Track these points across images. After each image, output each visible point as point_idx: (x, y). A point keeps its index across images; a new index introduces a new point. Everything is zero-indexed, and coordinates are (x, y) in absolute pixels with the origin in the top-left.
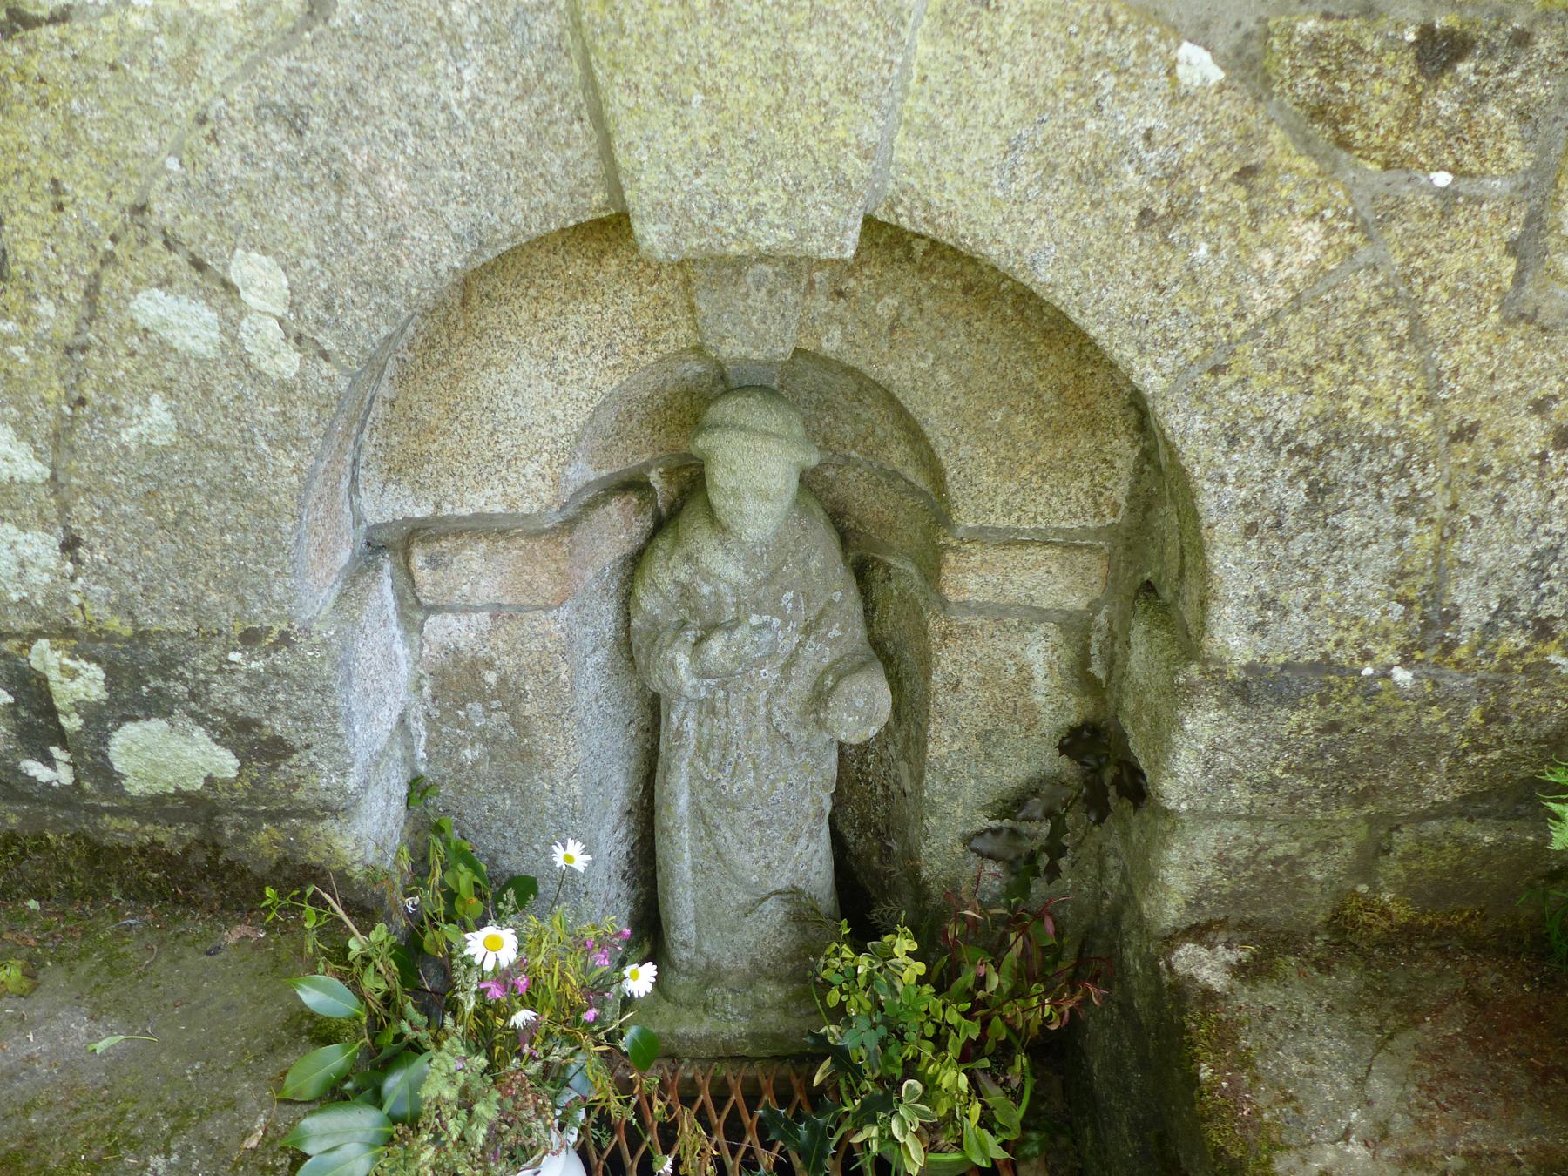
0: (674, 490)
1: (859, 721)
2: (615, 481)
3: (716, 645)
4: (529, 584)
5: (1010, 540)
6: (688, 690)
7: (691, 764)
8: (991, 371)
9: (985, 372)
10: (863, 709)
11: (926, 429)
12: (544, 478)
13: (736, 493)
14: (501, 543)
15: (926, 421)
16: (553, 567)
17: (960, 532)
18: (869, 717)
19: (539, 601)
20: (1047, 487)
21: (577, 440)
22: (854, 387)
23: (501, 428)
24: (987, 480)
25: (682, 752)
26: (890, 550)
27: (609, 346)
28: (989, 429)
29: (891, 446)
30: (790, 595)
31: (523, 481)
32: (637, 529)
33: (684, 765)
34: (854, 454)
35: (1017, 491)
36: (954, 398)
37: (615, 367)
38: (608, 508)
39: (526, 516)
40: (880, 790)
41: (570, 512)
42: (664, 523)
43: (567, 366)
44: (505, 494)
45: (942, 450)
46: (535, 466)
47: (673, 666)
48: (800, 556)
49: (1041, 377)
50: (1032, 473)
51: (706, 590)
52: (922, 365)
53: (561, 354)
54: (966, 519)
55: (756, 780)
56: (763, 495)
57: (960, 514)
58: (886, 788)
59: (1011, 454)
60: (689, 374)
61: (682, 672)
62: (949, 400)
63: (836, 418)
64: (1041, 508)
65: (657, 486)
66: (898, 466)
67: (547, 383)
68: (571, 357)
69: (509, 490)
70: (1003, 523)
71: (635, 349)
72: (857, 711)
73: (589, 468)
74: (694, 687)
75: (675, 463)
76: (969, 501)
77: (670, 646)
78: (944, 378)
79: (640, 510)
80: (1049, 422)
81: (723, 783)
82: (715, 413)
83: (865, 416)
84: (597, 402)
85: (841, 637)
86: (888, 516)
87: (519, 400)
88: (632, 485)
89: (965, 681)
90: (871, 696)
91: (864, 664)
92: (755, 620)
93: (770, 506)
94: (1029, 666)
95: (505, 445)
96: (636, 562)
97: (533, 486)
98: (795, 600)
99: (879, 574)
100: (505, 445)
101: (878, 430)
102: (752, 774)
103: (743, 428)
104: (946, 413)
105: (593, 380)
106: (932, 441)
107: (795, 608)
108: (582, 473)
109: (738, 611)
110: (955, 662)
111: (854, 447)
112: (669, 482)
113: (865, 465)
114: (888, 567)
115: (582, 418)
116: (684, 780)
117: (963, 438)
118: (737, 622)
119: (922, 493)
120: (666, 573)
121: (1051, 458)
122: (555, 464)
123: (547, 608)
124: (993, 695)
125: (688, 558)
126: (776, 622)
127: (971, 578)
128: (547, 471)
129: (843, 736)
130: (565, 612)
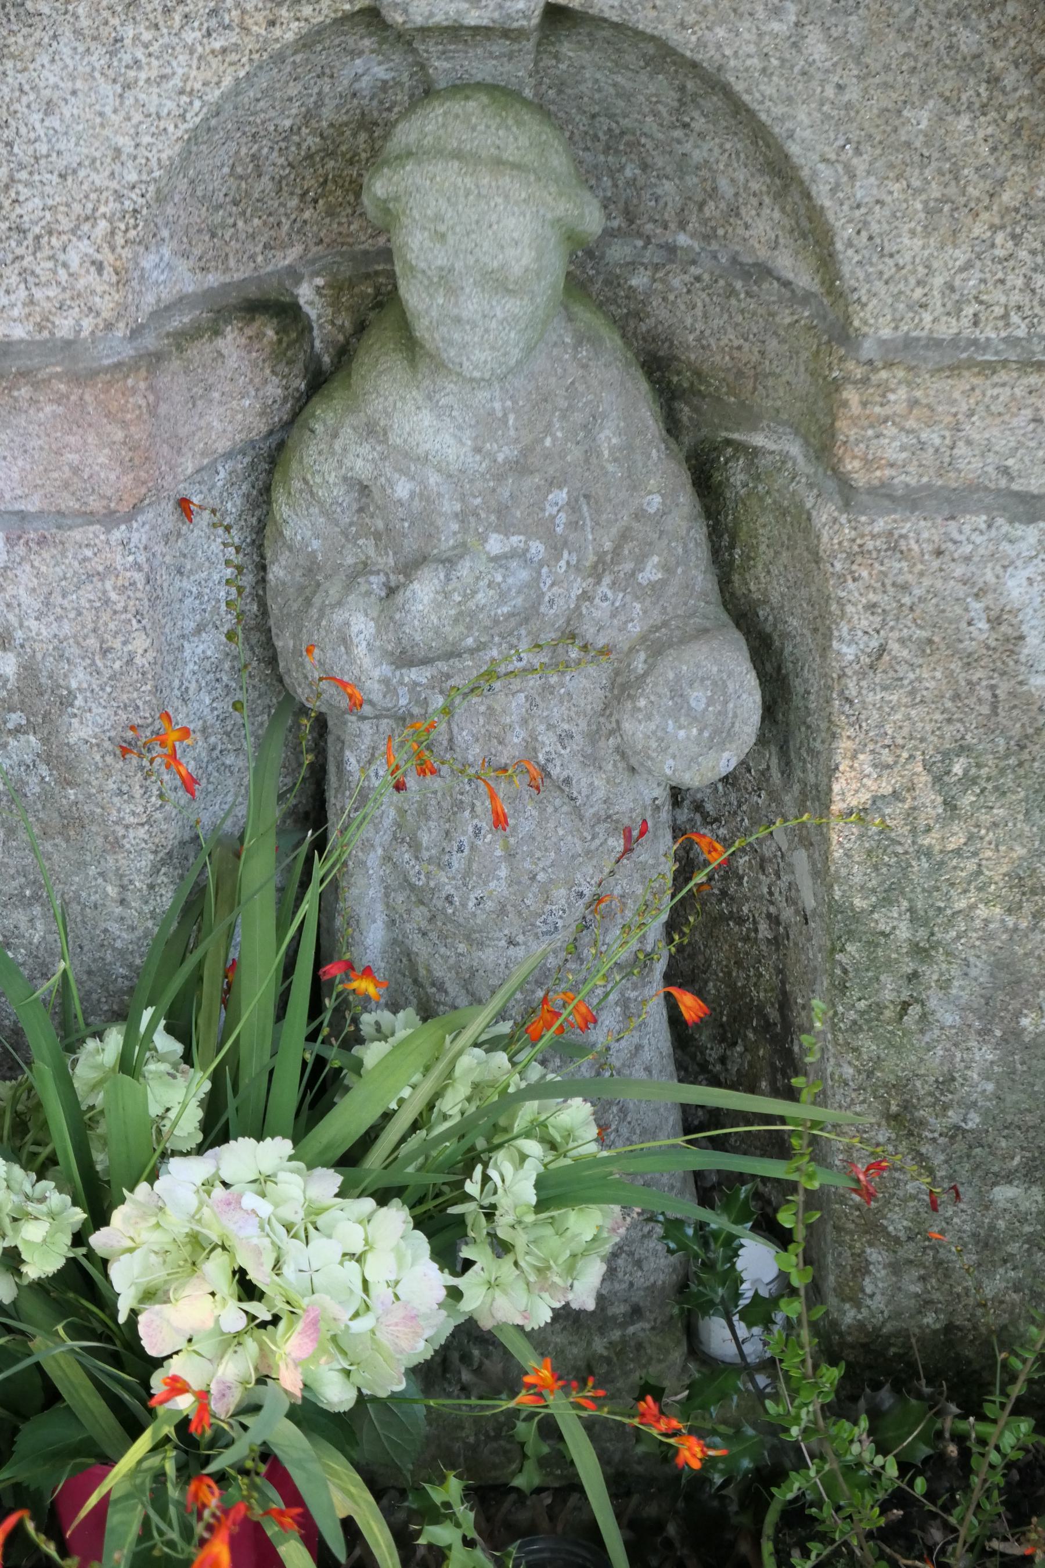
0: (345, 320)
1: (698, 741)
2: (233, 298)
3: (423, 591)
4: (76, 470)
5: (960, 359)
6: (373, 689)
7: (387, 859)
8: (903, 34)
9: (892, 35)
10: (701, 717)
11: (794, 149)
12: (100, 267)
13: (445, 281)
14: (24, 392)
15: (791, 136)
16: (119, 435)
17: (868, 349)
18: (717, 732)
19: (95, 504)
20: (1023, 254)
21: (161, 198)
22: (671, 97)
23: (23, 175)
24: (911, 246)
25: (367, 831)
26: (752, 419)
27: (214, 12)
28: (908, 144)
29: (748, 213)
30: (561, 496)
31: (62, 275)
32: (274, 390)
33: (373, 858)
34: (683, 239)
35: (968, 266)
36: (840, 87)
37: (224, 51)
38: (220, 343)
39: (68, 344)
40: (764, 930)
41: (150, 341)
42: (320, 378)
43: (140, 54)
44: (31, 301)
45: (824, 189)
46: (84, 246)
47: (345, 641)
48: (578, 417)
49: (994, 42)
50: (994, 228)
51: (402, 489)
52: (775, 26)
53: (129, 32)
54: (877, 322)
55: (512, 882)
56: (497, 283)
57: (867, 314)
58: (774, 920)
59: (952, 190)
60: (364, 82)
61: (360, 650)
62: (830, 92)
63: (645, 167)
64: (1016, 298)
65: (313, 313)
66: (763, 253)
67: (107, 89)
68: (147, 36)
69: (39, 294)
70: (947, 329)
71: (260, 17)
72: (694, 718)
73: (183, 266)
74: (385, 681)
75: (346, 270)
76: (879, 286)
77: (340, 603)
78: (817, 48)
79: (279, 355)
80: (1017, 128)
81: (449, 889)
82: (406, 134)
83: (697, 156)
84: (192, 121)
85: (663, 583)
86: (750, 354)
87: (54, 122)
88: (269, 308)
89: (894, 646)
90: (719, 686)
91: (706, 631)
92: (495, 544)
93: (513, 306)
94: (1015, 612)
95: (31, 208)
96: (271, 459)
97: (81, 284)
98: (572, 506)
99: (737, 475)
100: (31, 208)
101: (723, 183)
102: (503, 872)
103: (457, 155)
104: (828, 117)
105: (186, 79)
106: (805, 173)
107: (574, 525)
108: (173, 275)
109: (465, 530)
110: (871, 607)
111: (682, 225)
112: (335, 304)
113: (705, 259)
114: (753, 453)
115: (168, 151)
116: (374, 892)
117: (860, 165)
118: (463, 550)
119: (807, 298)
120: (335, 456)
121: (1028, 195)
122: (119, 240)
123: (110, 519)
124: (950, 675)
125: (372, 431)
126: (537, 548)
127: (889, 434)
128: (107, 256)
129: (670, 768)
130: (139, 535)
